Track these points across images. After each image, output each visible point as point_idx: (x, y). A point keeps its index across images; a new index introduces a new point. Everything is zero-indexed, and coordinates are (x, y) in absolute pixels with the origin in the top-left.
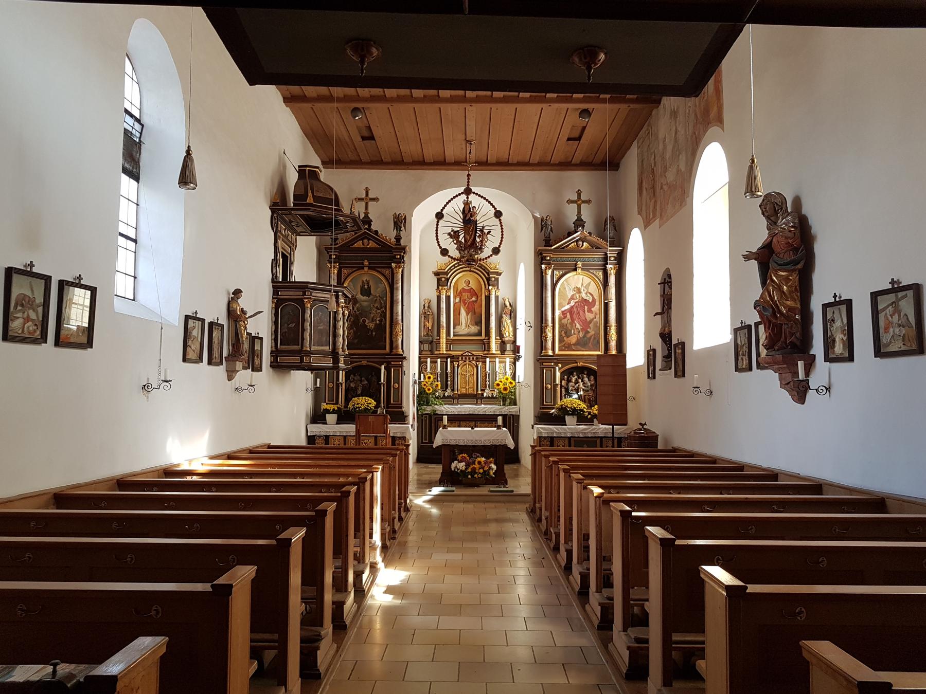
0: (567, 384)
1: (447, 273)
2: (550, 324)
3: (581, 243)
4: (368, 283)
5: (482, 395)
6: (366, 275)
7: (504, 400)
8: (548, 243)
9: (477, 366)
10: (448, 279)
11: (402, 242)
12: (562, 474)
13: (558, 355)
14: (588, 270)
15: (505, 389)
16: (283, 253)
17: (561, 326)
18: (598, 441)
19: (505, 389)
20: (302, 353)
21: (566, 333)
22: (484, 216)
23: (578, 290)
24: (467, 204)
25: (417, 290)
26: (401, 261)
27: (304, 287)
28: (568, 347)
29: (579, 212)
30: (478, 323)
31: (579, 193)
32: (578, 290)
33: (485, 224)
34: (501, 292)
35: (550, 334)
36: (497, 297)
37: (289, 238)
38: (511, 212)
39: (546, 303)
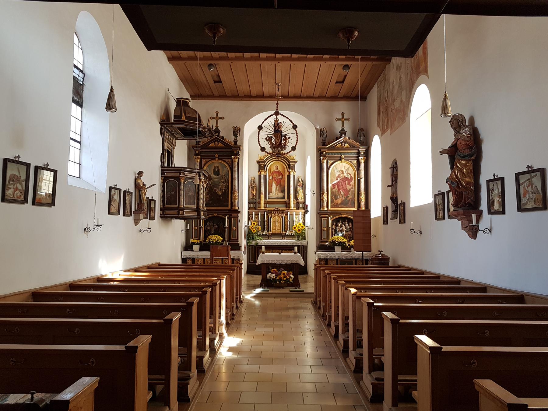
0: (336, 228)
1: (264, 162)
2: (325, 192)
3: (344, 144)
4: (218, 167)
5: (286, 234)
6: (216, 163)
7: (298, 237)
8: (324, 144)
9: (282, 217)
10: (265, 166)
11: (238, 143)
12: (333, 281)
13: (330, 210)
14: (348, 160)
15: (299, 230)
16: (167, 150)
17: (332, 193)
18: (354, 261)
19: (299, 230)
20: (179, 209)
21: (335, 197)
22: (287, 128)
23: (342, 172)
24: (276, 121)
25: (247, 172)
26: (237, 155)
27: (180, 170)
28: (336, 206)
29: (343, 125)
30: (283, 191)
31: (343, 114)
32: (342, 172)
33: (287, 132)
34: (297, 173)
35: (325, 198)
36: (294, 176)
37: (171, 141)
38: (302, 126)
39: (323, 180)
